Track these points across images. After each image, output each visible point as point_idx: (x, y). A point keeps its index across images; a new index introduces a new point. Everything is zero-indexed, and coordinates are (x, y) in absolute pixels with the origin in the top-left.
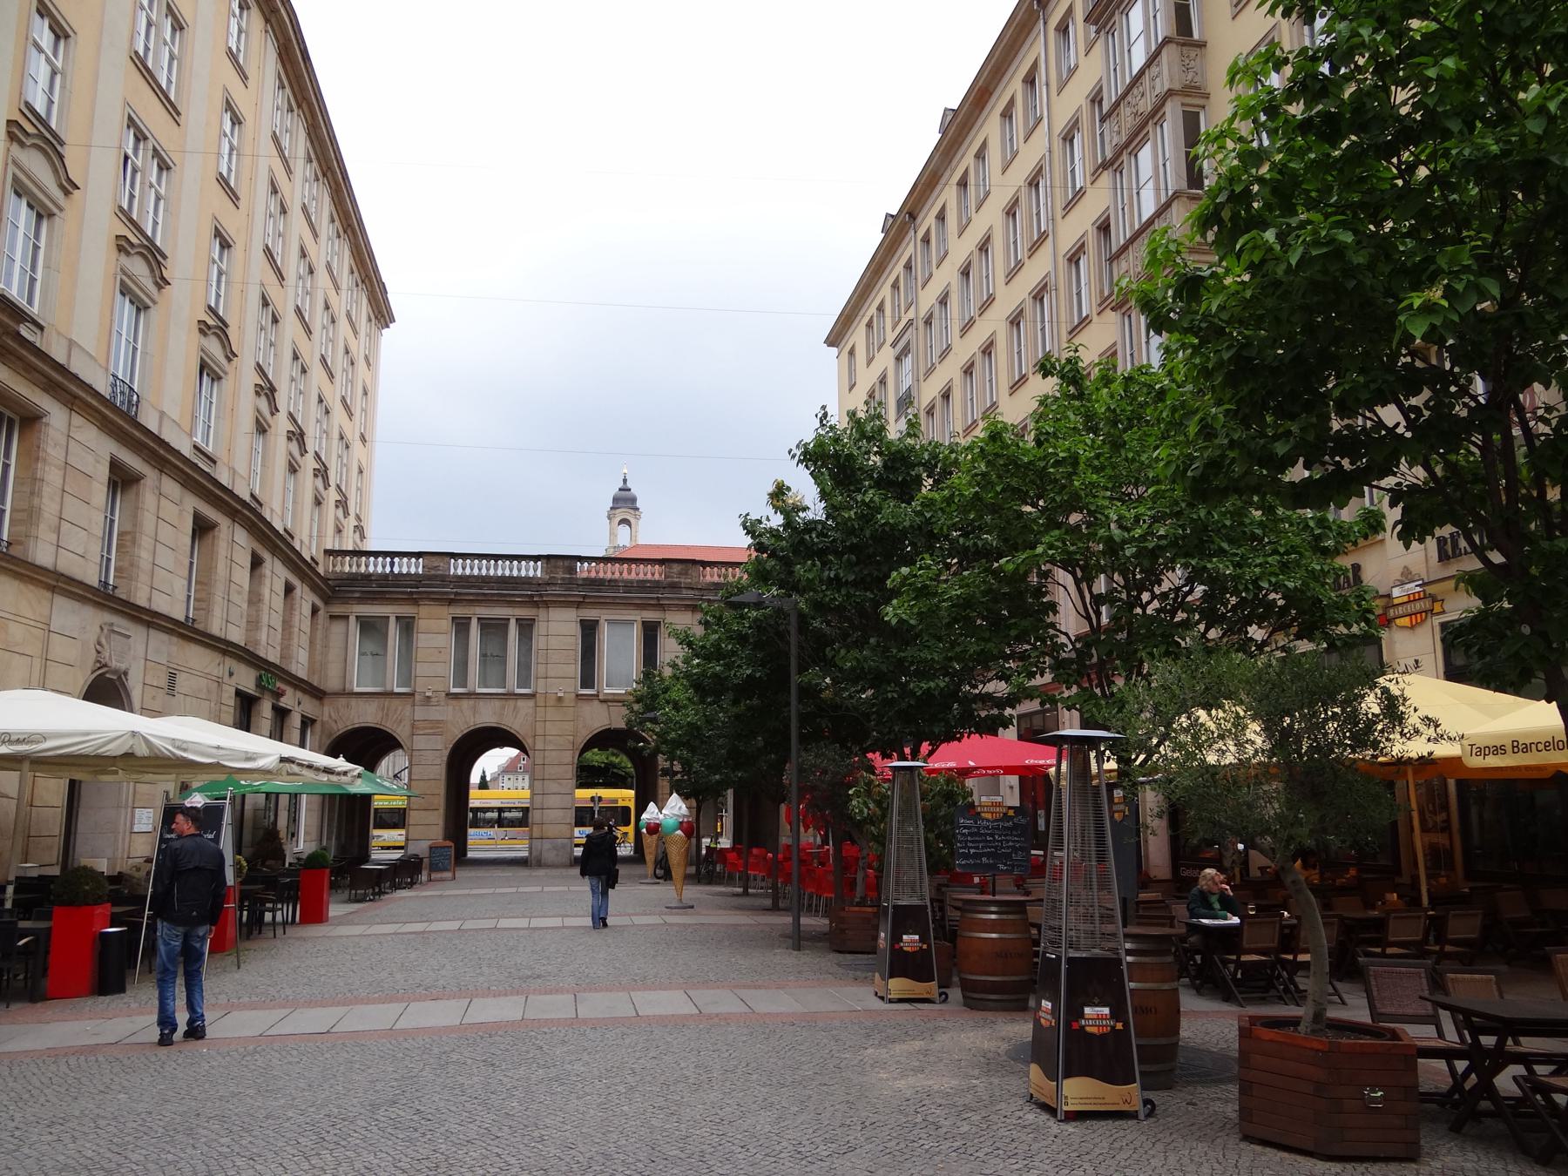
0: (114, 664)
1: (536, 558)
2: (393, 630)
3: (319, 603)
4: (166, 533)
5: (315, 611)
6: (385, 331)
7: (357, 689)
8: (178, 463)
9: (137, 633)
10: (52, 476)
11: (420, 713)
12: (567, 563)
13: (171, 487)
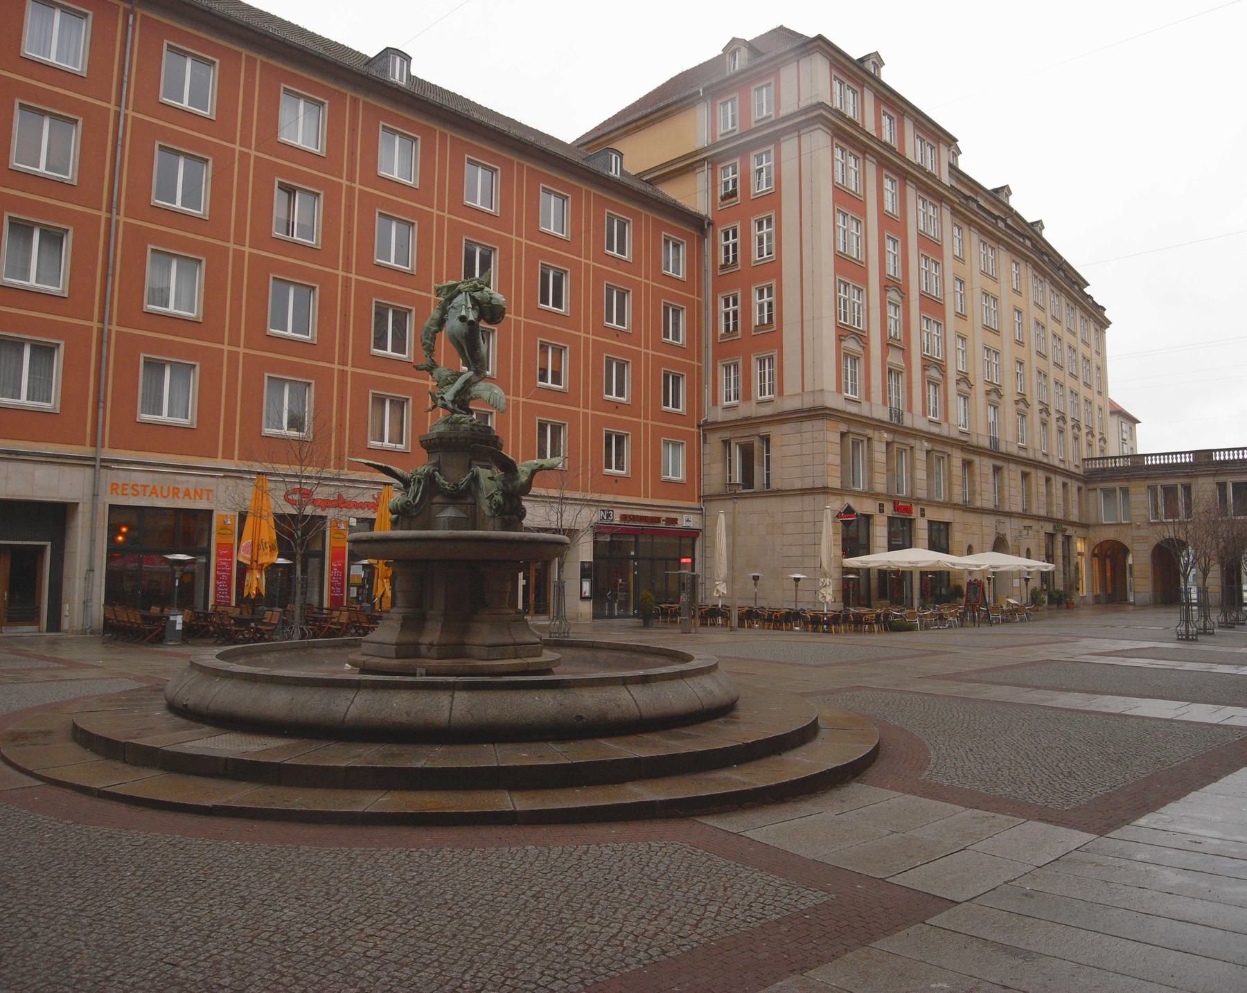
0: (1001, 532)
1: (1189, 452)
2: (1119, 493)
3: (1081, 485)
4: (1013, 483)
5: (1079, 489)
7: (1104, 522)
9: (1007, 520)
10: (977, 478)
11: (1135, 533)
12: (1206, 454)
13: (1012, 466)
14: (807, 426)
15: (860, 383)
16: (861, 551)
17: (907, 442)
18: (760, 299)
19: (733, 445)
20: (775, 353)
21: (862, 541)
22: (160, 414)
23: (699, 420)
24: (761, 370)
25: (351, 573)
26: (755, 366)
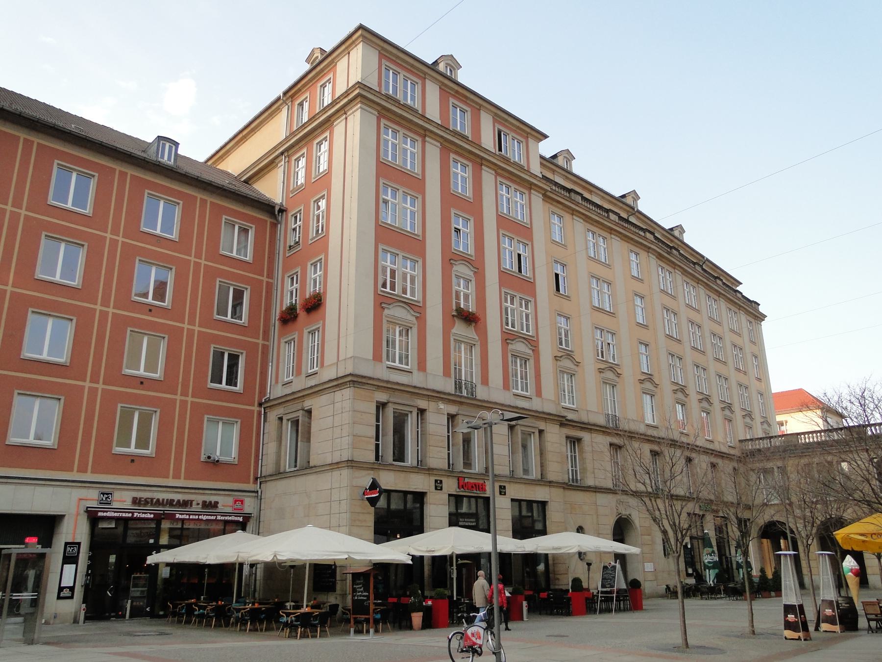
0: (624, 513)
6: (763, 323)
8: (67, 342)
10: (588, 456)
15: (531, 381)
16: (414, 532)
17: (414, 404)
19: (284, 421)
21: (416, 523)
22: (129, 447)
23: (260, 398)
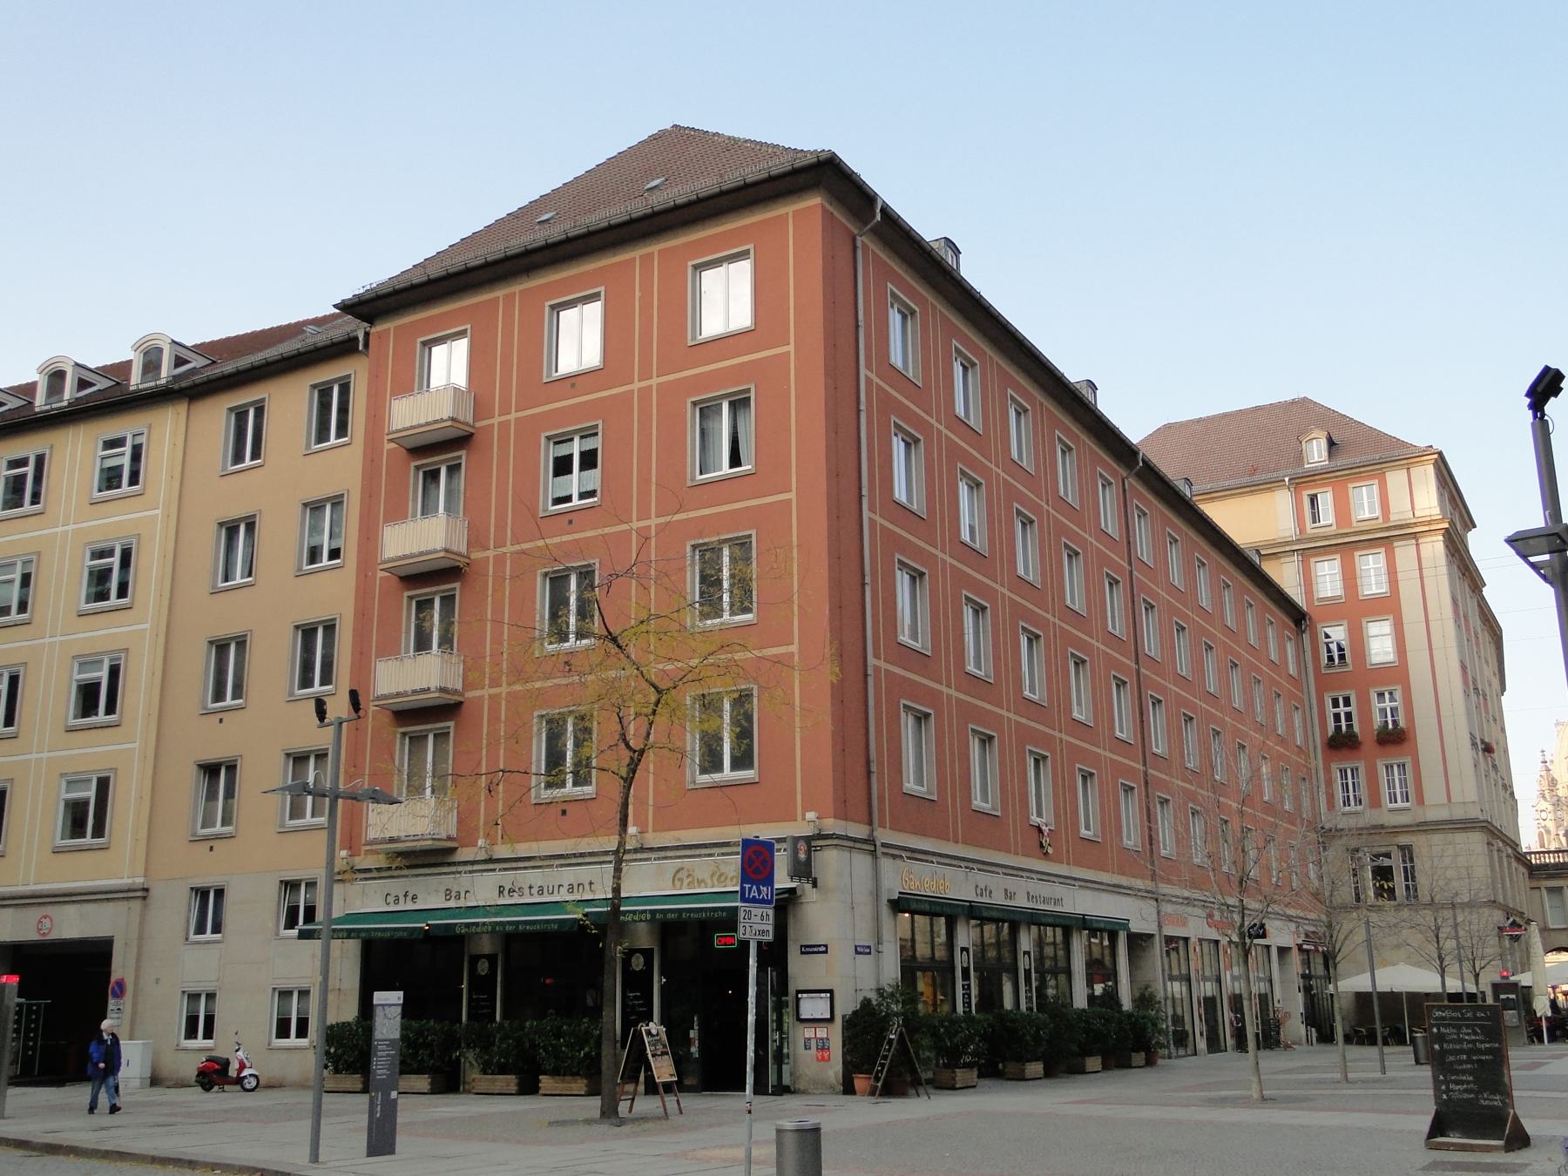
7: (1551, 927)
14: (1460, 837)
18: (1334, 707)
20: (1408, 760)
24: (1388, 776)
25: (1369, 974)
26: (1382, 771)
